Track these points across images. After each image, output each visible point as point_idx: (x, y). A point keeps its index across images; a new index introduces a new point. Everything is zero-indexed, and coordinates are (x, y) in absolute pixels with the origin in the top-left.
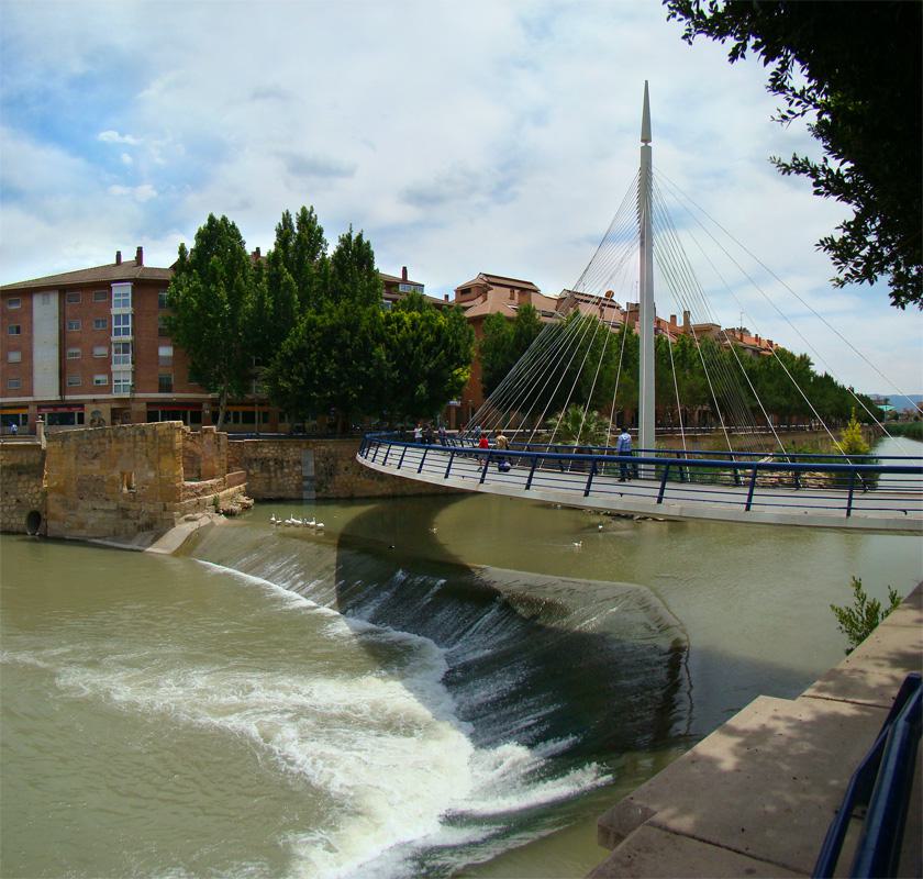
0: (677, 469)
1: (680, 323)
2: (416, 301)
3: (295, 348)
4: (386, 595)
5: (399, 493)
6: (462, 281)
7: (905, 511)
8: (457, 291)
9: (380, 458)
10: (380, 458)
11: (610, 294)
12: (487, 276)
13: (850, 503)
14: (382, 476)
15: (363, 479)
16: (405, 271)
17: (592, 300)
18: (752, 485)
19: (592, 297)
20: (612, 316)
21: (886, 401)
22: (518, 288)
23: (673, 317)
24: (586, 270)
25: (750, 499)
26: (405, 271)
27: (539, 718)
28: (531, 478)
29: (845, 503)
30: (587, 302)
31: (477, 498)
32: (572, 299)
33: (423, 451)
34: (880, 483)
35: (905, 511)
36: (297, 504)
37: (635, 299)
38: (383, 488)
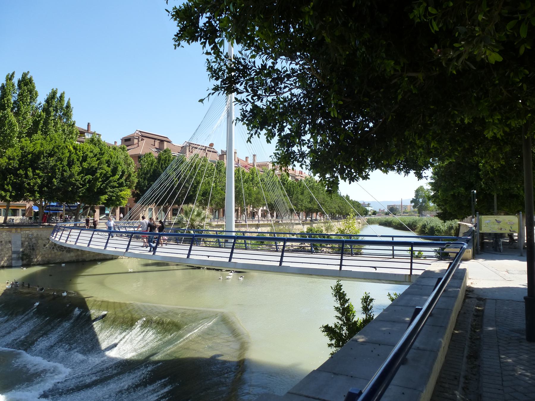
0: (243, 241)
1: (250, 161)
2: (95, 141)
3: (289, 62)
4: (67, 325)
5: (80, 260)
6: (126, 134)
7: (375, 268)
8: (122, 140)
9: (58, 237)
10: (58, 237)
11: (211, 145)
12: (141, 132)
13: (341, 262)
14: (69, 250)
15: (56, 251)
16: (89, 125)
17: (199, 147)
18: (283, 251)
19: (199, 145)
20: (211, 157)
21: (369, 205)
22: (158, 140)
23: (247, 158)
24: (197, 129)
25: (282, 259)
26: (89, 125)
27: (158, 396)
28: (190, 250)
29: (338, 262)
30: (196, 148)
31: (432, 290)
32: (190, 146)
33: (79, 231)
34: (363, 251)
35: (375, 268)
36: (450, 339)
37: (225, 149)
38: (68, 256)
